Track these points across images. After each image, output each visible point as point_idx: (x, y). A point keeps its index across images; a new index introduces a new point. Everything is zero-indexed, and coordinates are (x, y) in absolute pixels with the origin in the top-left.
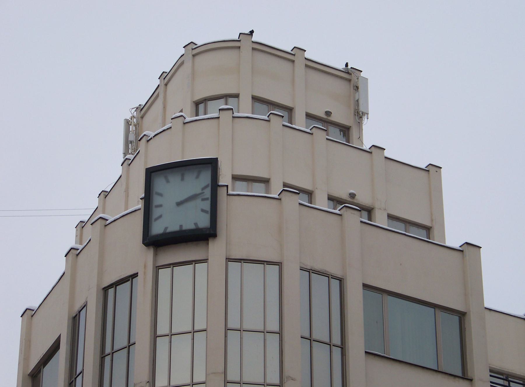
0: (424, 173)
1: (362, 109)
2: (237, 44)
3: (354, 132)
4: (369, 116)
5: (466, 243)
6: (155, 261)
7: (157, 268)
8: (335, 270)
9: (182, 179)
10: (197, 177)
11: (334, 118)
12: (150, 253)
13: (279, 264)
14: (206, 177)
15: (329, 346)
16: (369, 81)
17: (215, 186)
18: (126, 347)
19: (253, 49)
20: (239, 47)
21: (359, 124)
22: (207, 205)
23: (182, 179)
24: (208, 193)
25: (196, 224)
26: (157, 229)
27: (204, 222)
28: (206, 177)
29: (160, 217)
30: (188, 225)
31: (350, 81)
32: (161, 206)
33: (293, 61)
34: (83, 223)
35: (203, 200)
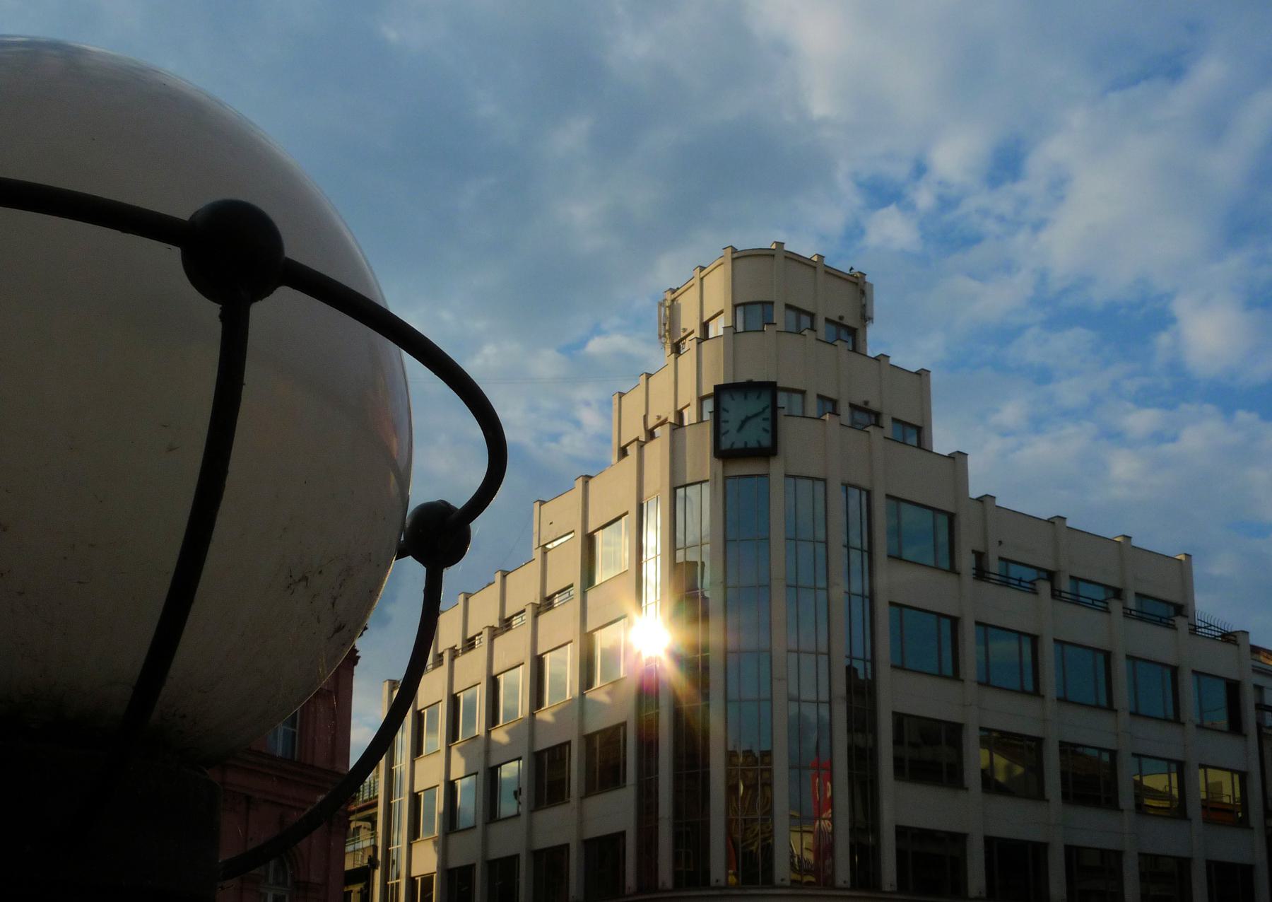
0: (875, 362)
1: (868, 314)
2: (772, 253)
3: (860, 333)
4: (874, 320)
5: (958, 452)
6: (724, 472)
7: (725, 478)
8: (865, 483)
9: (746, 398)
10: (758, 397)
11: (845, 322)
12: (719, 464)
13: (825, 480)
14: (765, 400)
15: (822, 483)
16: (874, 286)
17: (775, 408)
18: (721, 312)
19: (786, 257)
20: (773, 256)
21: (865, 327)
22: (767, 425)
23: (746, 398)
24: (768, 414)
25: (759, 442)
26: (726, 444)
27: (766, 441)
28: (765, 400)
29: (727, 432)
30: (752, 444)
31: (857, 284)
32: (727, 422)
33: (815, 268)
34: (565, 647)
35: (764, 419)
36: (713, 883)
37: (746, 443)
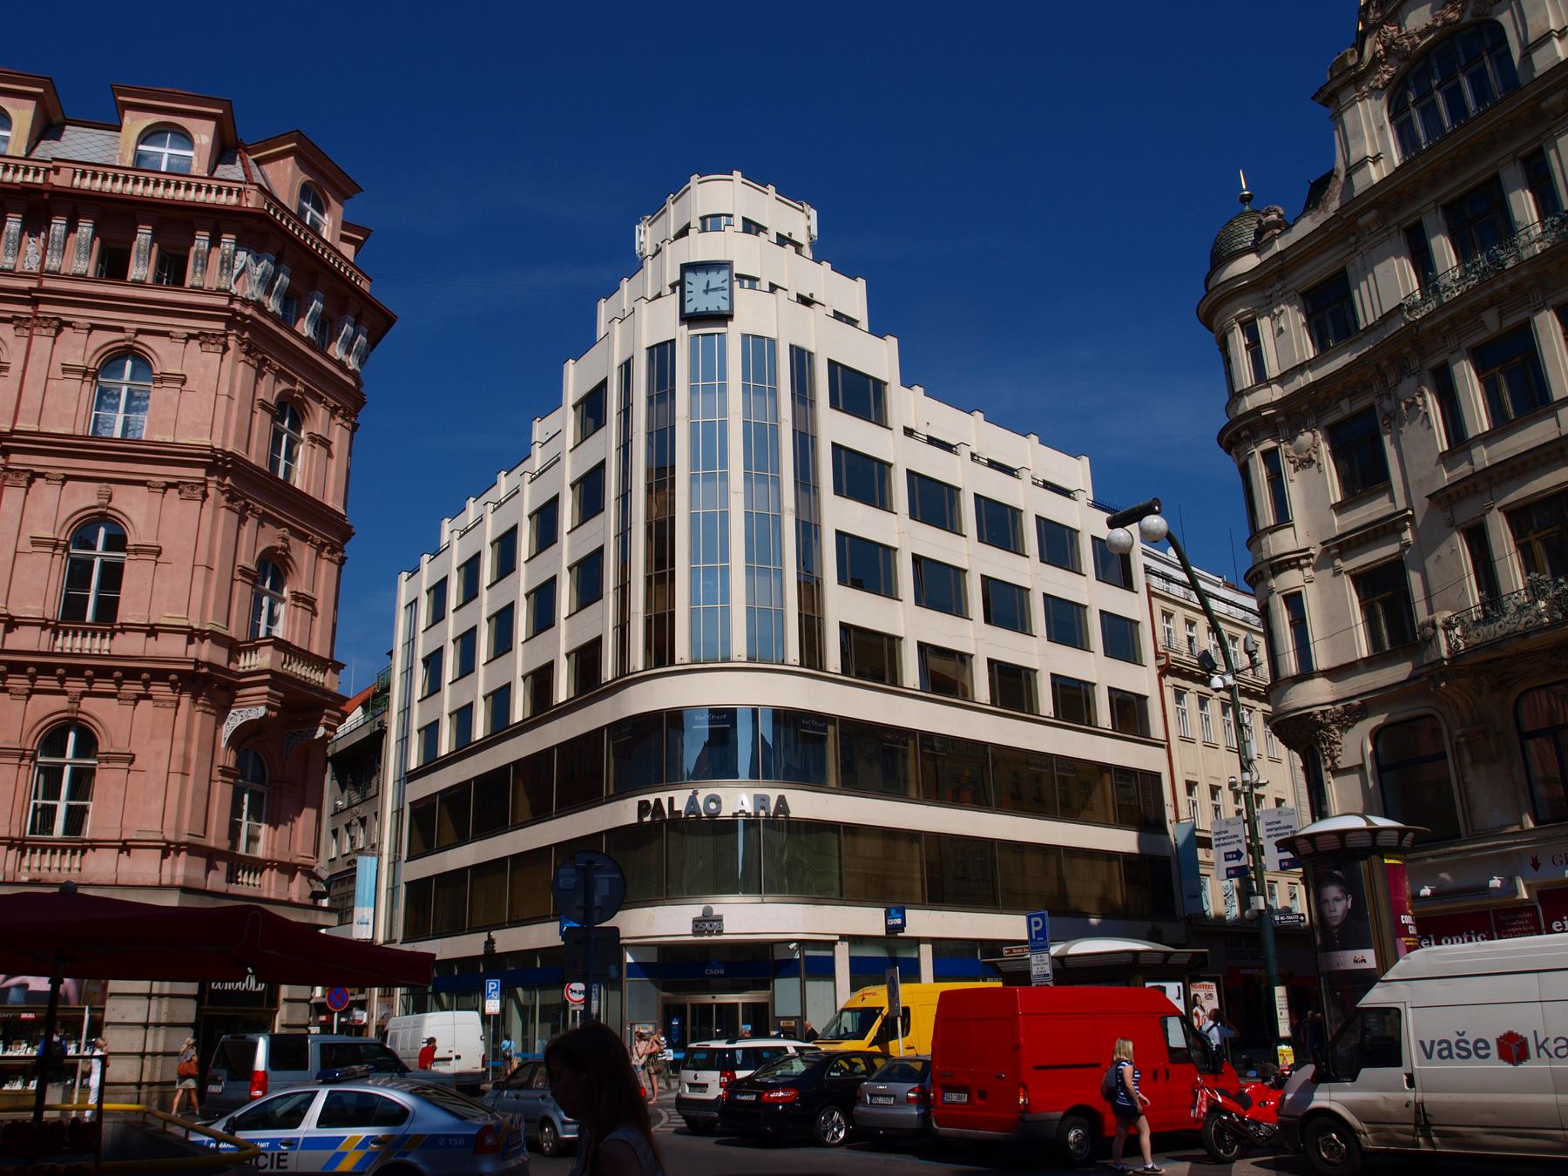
26: (689, 309)
36: (677, 661)
37: (707, 308)
